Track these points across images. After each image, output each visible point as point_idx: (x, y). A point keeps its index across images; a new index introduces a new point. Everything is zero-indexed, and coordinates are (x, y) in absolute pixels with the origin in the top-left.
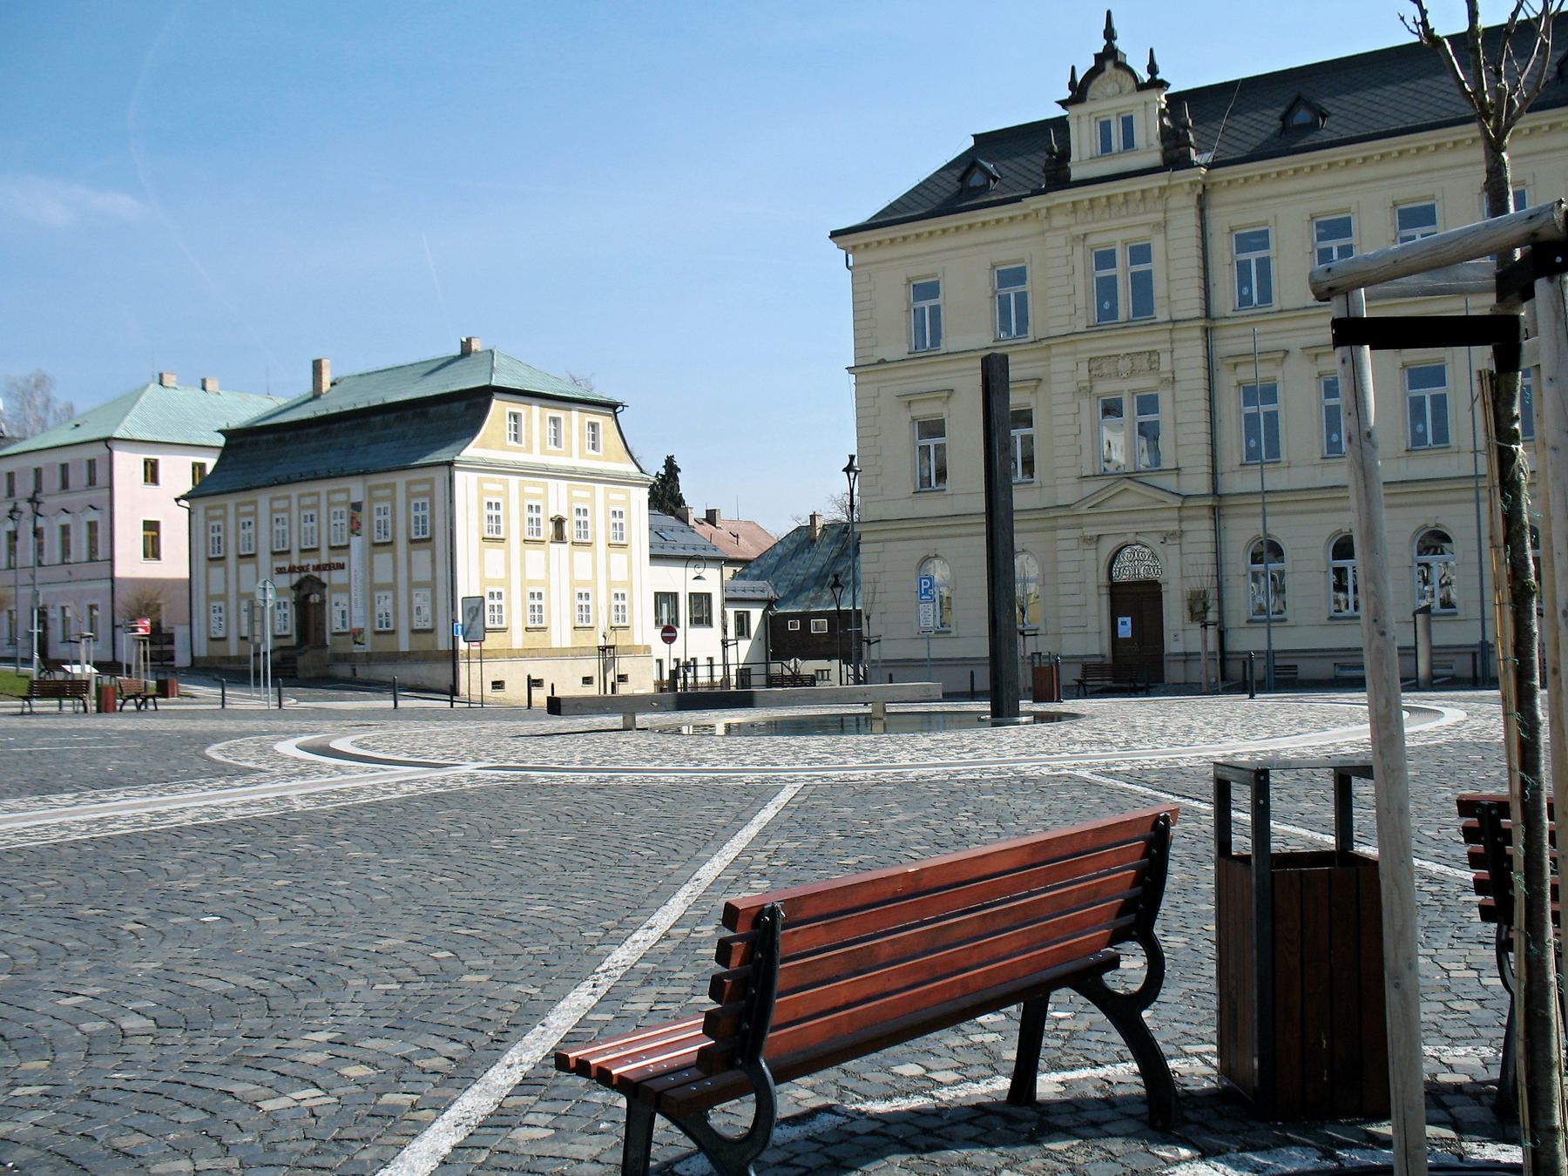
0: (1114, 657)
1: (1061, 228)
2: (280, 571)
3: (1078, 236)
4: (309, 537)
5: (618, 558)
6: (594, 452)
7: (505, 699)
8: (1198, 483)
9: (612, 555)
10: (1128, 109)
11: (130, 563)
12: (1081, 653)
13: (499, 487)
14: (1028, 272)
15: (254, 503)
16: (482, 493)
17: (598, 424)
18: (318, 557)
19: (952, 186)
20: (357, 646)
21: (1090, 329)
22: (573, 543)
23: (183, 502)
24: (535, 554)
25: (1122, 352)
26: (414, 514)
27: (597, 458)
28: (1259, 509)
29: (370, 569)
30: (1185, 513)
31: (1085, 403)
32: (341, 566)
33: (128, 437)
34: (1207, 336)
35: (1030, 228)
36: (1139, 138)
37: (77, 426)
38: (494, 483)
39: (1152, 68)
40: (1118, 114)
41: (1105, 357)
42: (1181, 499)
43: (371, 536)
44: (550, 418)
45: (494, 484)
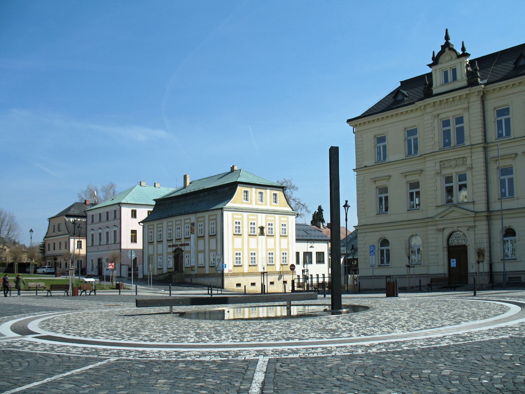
0: (449, 274)
1: (429, 113)
2: (170, 246)
3: (436, 115)
4: (178, 234)
5: (284, 241)
6: (275, 204)
7: (241, 290)
8: (481, 207)
9: (281, 239)
10: (455, 65)
11: (126, 243)
12: (437, 273)
13: (240, 217)
14: (418, 129)
15: (162, 224)
16: (233, 218)
17: (277, 194)
18: (181, 242)
19: (391, 101)
20: (193, 272)
21: (440, 150)
22: (267, 235)
23: (141, 224)
24: (253, 240)
25: (452, 158)
26: (211, 226)
27: (277, 206)
28: (500, 217)
29: (197, 245)
30: (476, 219)
31: (438, 178)
32: (188, 245)
33: (126, 202)
34: (485, 150)
35: (418, 113)
36: (459, 76)
37: (113, 199)
39: (463, 49)
40: (451, 68)
41: (446, 160)
42: (474, 213)
43: (197, 235)
44: (259, 192)
45: (238, 216)
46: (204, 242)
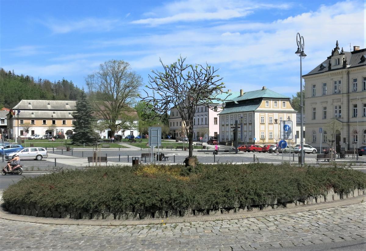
2: (232, 128)
23: (218, 115)
24: (271, 126)
27: (285, 108)
38: (262, 114)
46: (252, 126)
